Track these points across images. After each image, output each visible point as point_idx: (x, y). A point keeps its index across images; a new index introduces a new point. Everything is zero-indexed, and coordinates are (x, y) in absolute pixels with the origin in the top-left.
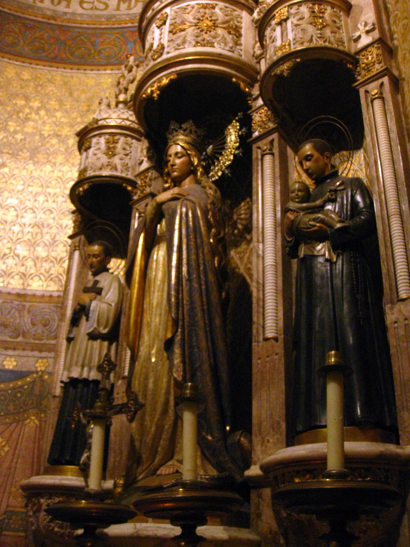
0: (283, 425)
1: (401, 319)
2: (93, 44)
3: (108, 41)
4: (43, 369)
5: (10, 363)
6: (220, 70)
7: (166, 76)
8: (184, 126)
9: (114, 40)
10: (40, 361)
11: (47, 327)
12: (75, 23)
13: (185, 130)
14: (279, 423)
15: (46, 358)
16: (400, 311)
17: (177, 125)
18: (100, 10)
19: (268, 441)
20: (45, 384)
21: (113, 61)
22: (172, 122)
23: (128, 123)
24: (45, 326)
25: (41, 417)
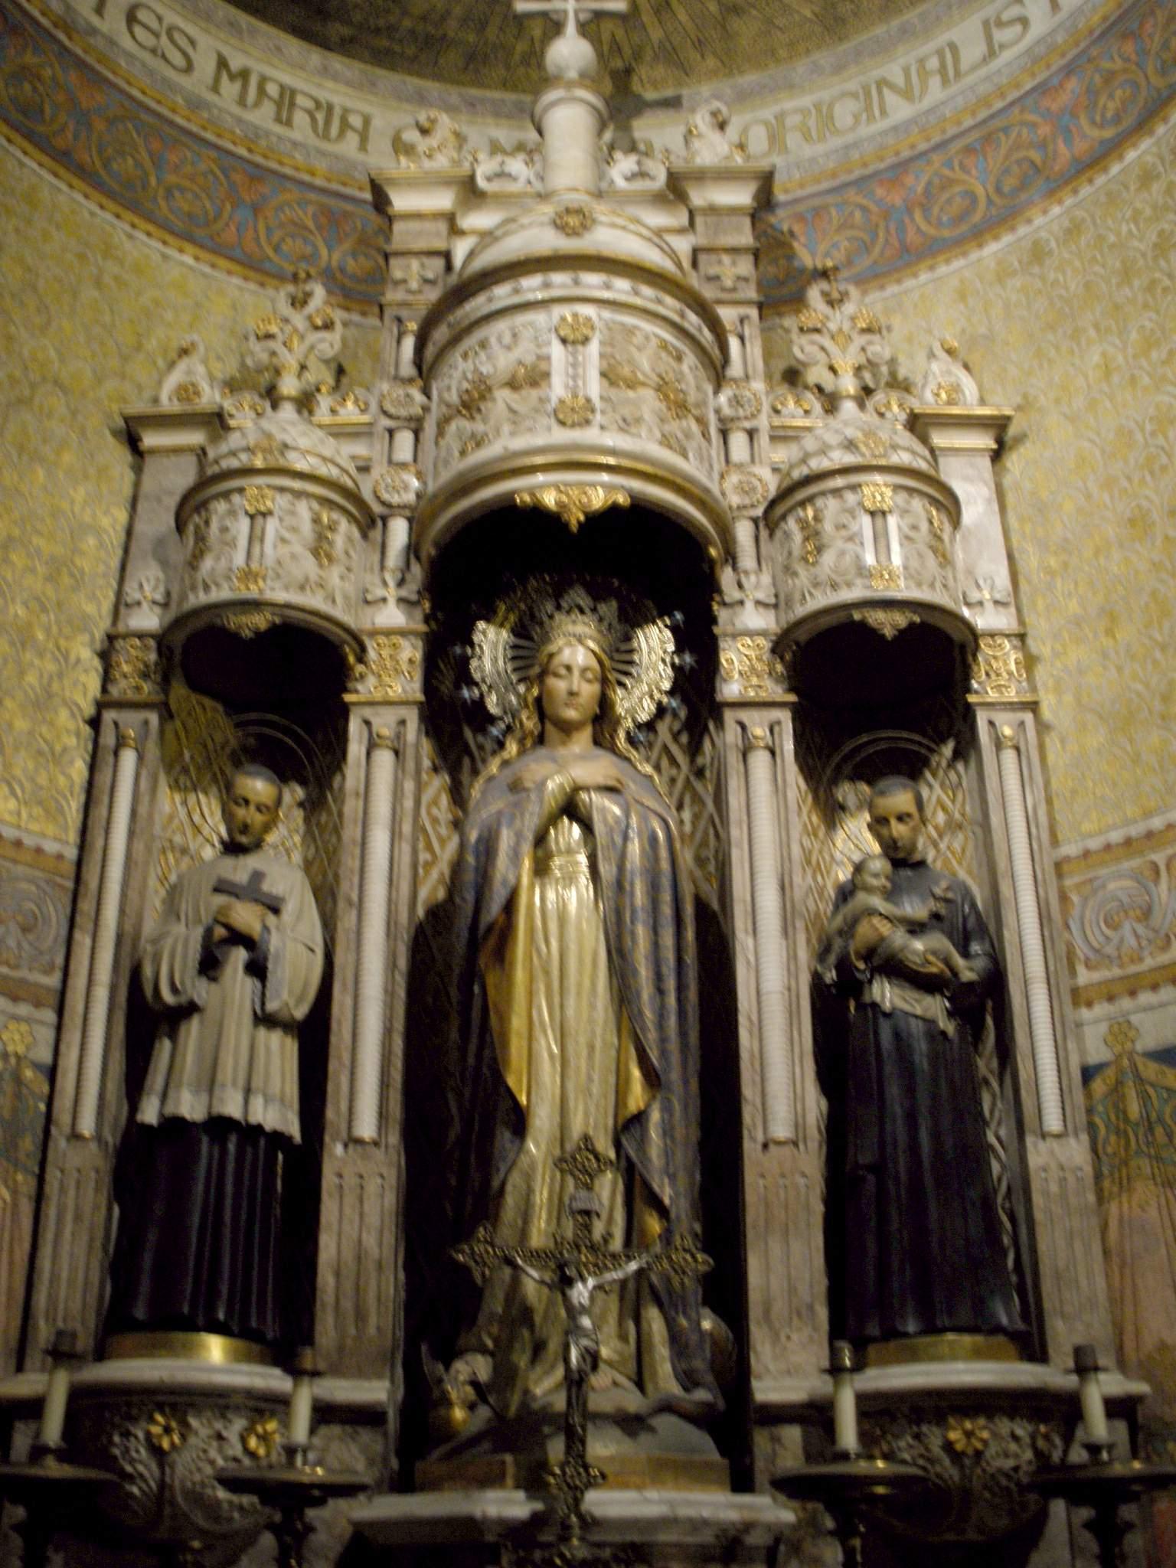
0: (822, 1313)
1: (1053, 1166)
2: (157, 162)
3: (189, 169)
4: (21, 1049)
5: (17, 1037)
6: (689, 520)
7: (608, 488)
8: (603, 608)
9: (205, 175)
10: (13, 1026)
11: (31, 937)
12: (114, 73)
13: (601, 620)
14: (811, 1308)
15: (28, 1020)
16: (1052, 1152)
17: (584, 600)
18: (174, 67)
19: (788, 1338)
20: (25, 1091)
21: (200, 233)
22: (614, 604)
23: (334, 472)
24: (25, 930)
25: (15, 1181)
